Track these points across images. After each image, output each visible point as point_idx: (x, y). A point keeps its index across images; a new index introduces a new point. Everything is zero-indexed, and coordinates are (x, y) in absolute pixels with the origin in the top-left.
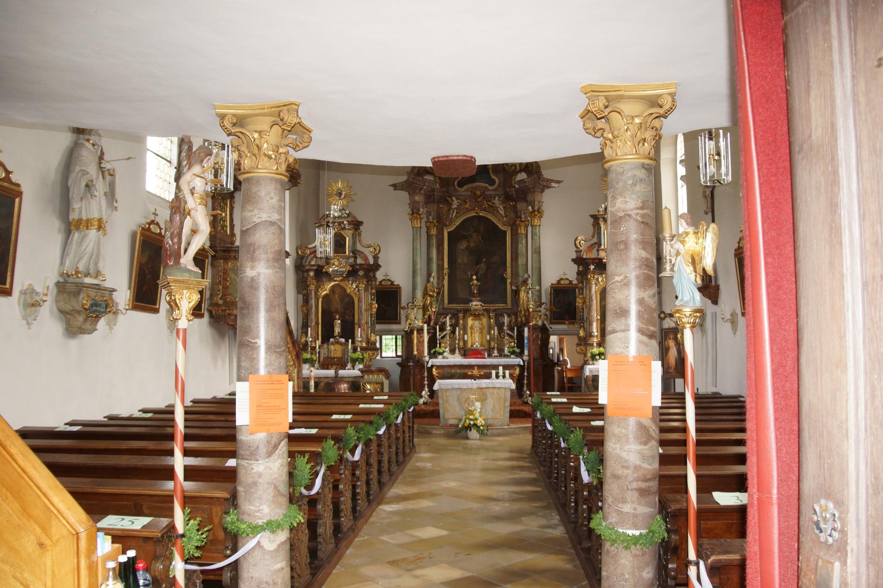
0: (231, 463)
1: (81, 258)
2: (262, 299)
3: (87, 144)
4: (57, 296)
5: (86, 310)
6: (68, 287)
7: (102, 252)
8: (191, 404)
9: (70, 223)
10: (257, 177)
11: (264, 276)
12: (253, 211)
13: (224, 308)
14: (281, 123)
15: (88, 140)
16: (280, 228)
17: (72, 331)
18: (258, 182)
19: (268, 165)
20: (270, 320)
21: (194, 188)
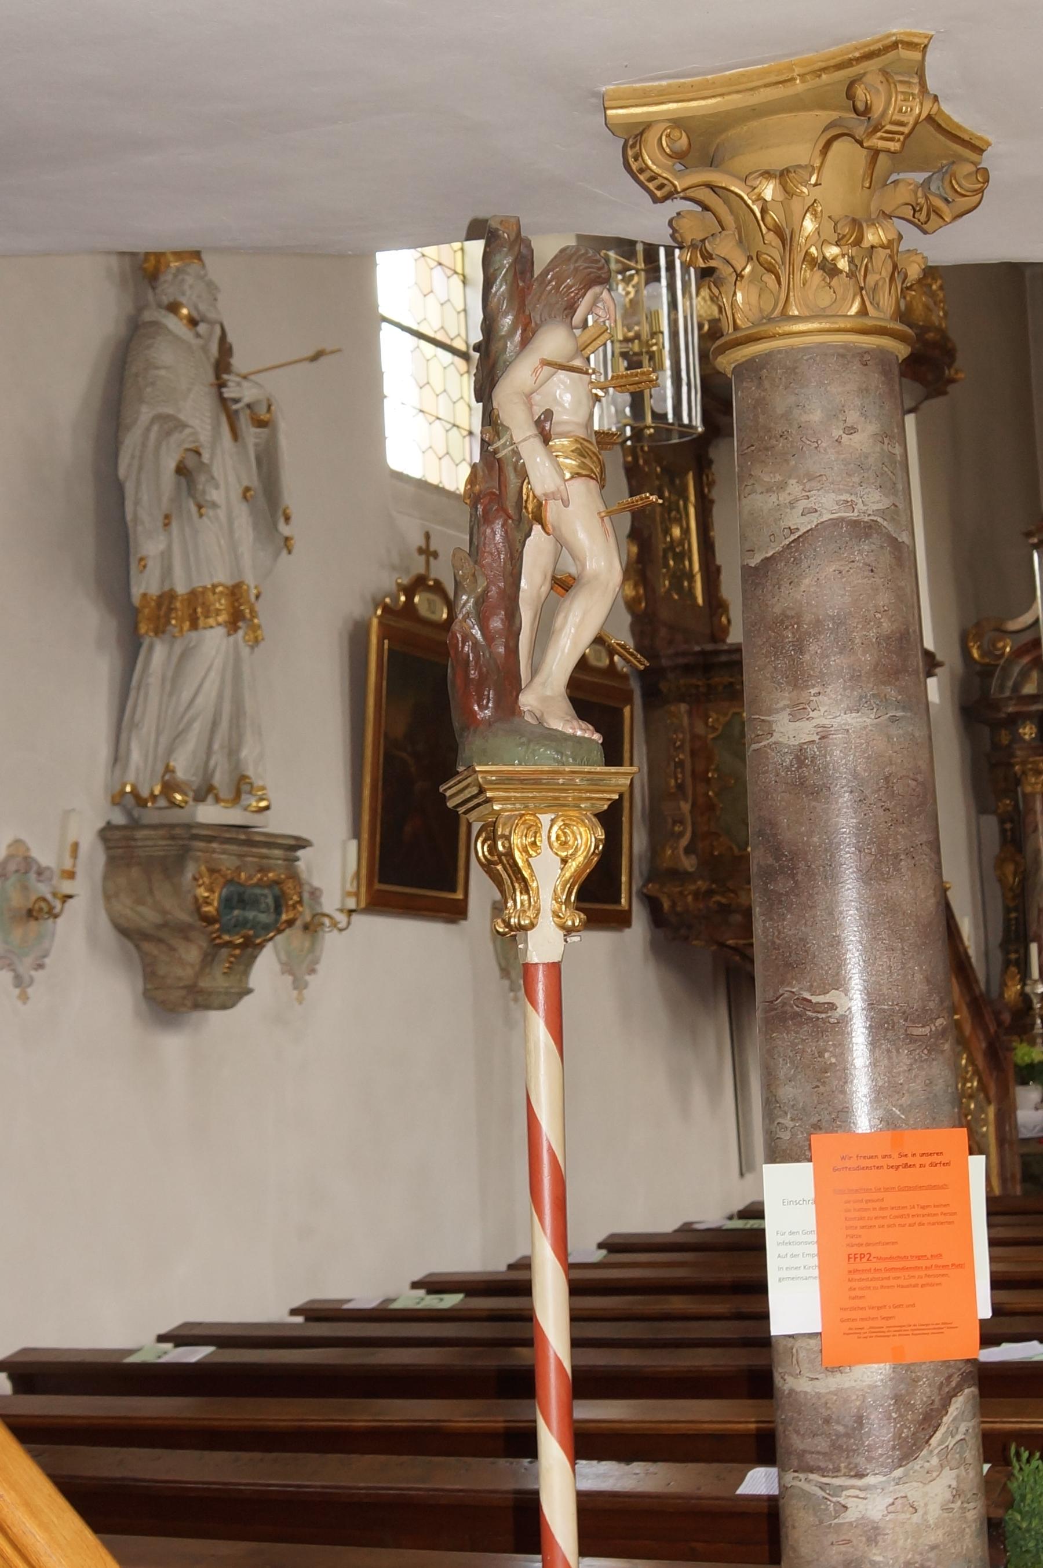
0: (759, 1481)
1: (178, 737)
2: (845, 822)
3: (172, 323)
4: (106, 877)
5: (208, 920)
6: (144, 843)
7: (249, 706)
8: (598, 1255)
9: (136, 611)
10: (789, 351)
11: (838, 734)
12: (782, 486)
13: (702, 885)
14: (860, 131)
15: (173, 308)
16: (894, 542)
17: (171, 1000)
18: (793, 370)
19: (825, 299)
20: (882, 915)
21: (548, 414)
